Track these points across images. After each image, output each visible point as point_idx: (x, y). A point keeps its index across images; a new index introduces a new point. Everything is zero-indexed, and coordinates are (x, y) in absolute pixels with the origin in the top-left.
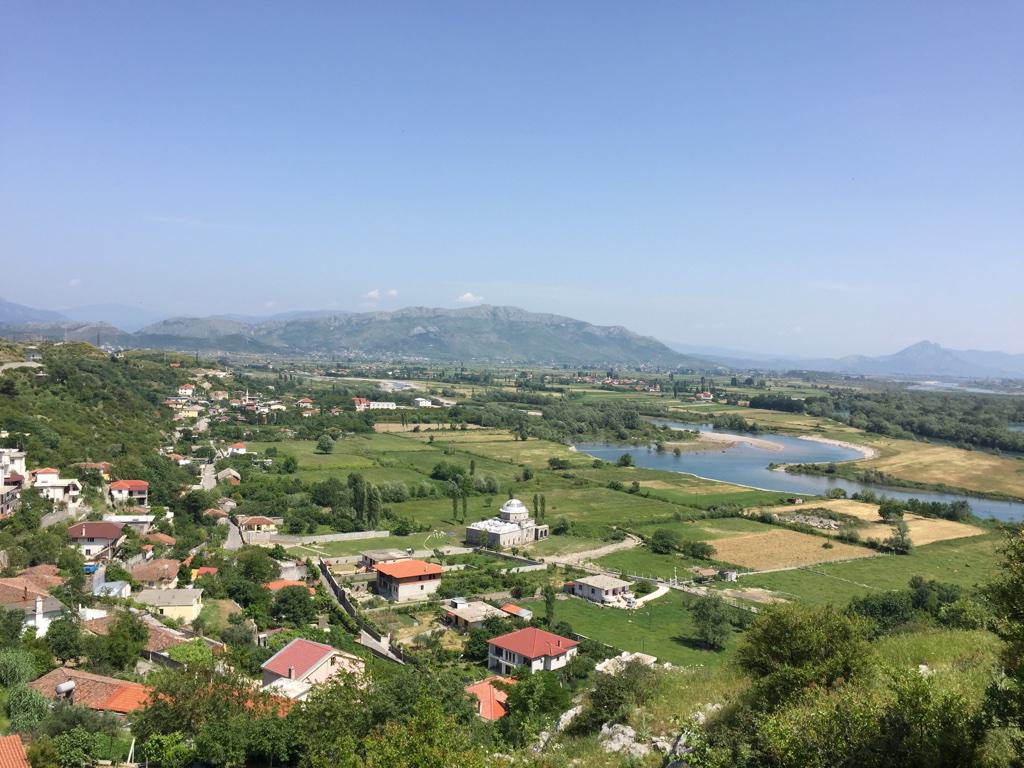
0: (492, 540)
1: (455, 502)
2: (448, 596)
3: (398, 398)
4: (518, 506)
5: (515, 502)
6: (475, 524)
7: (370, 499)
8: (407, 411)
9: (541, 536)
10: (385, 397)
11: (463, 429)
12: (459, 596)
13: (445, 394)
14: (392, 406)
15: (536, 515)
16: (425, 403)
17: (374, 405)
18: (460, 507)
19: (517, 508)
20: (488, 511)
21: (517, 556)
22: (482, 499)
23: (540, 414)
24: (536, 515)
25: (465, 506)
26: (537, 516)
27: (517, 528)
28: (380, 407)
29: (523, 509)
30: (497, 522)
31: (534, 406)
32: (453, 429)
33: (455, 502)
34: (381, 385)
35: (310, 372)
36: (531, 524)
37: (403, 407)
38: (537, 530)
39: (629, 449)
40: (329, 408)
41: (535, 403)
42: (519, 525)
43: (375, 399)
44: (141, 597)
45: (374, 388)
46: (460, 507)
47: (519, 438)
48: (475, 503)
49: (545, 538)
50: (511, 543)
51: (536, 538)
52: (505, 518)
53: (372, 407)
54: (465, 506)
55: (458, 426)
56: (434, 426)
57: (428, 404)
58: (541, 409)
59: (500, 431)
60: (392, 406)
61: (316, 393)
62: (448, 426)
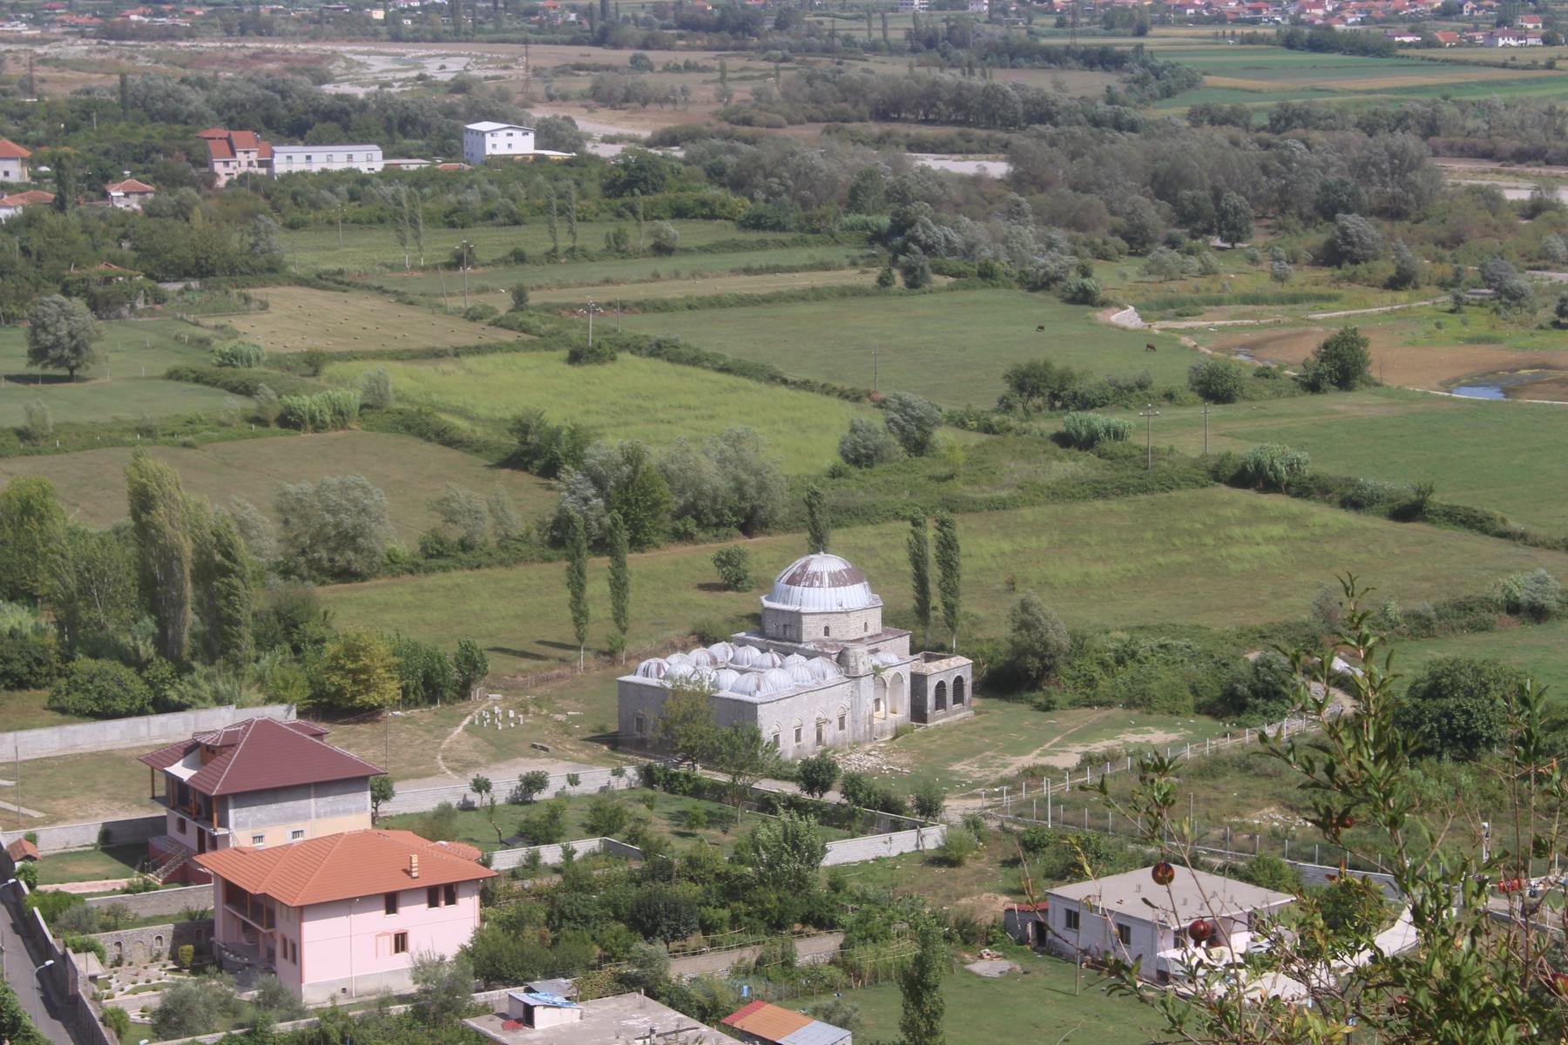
0: (731, 731)
1: (577, 582)
2: (231, 124)
3: (394, 124)
4: (837, 580)
5: (827, 564)
6: (653, 663)
7: (207, 572)
8: (436, 193)
9: (940, 702)
10: (340, 122)
11: (662, 249)
12: (550, 974)
13: (603, 98)
14: (368, 159)
15: (923, 610)
16: (506, 142)
17: (291, 159)
18: (597, 588)
19: (833, 593)
20: (733, 603)
21: (836, 794)
22: (700, 556)
23: (998, 168)
24: (923, 610)
25: (619, 586)
26: (923, 616)
27: (832, 673)
28: (316, 168)
29: (857, 595)
30: (752, 653)
31: (769, 236)
32: (617, 248)
33: (577, 582)
34: (337, 68)
35: (35, 22)
36: (896, 655)
37: (413, 165)
38: (918, 681)
39: (1360, 309)
40: (99, 182)
41: (976, 118)
42: (842, 659)
43: (298, 131)
44: (1149, 42)
45: (305, 83)
46: (597, 588)
47: (899, 280)
48: (669, 569)
49: (957, 714)
50: (809, 737)
51: (918, 713)
52: (781, 633)
53: (281, 166)
54: (619, 586)
55: (639, 235)
56: (534, 238)
57: (522, 144)
58: (1005, 146)
59: (820, 253)
60: (368, 159)
61: (51, 112)
62: (593, 237)
